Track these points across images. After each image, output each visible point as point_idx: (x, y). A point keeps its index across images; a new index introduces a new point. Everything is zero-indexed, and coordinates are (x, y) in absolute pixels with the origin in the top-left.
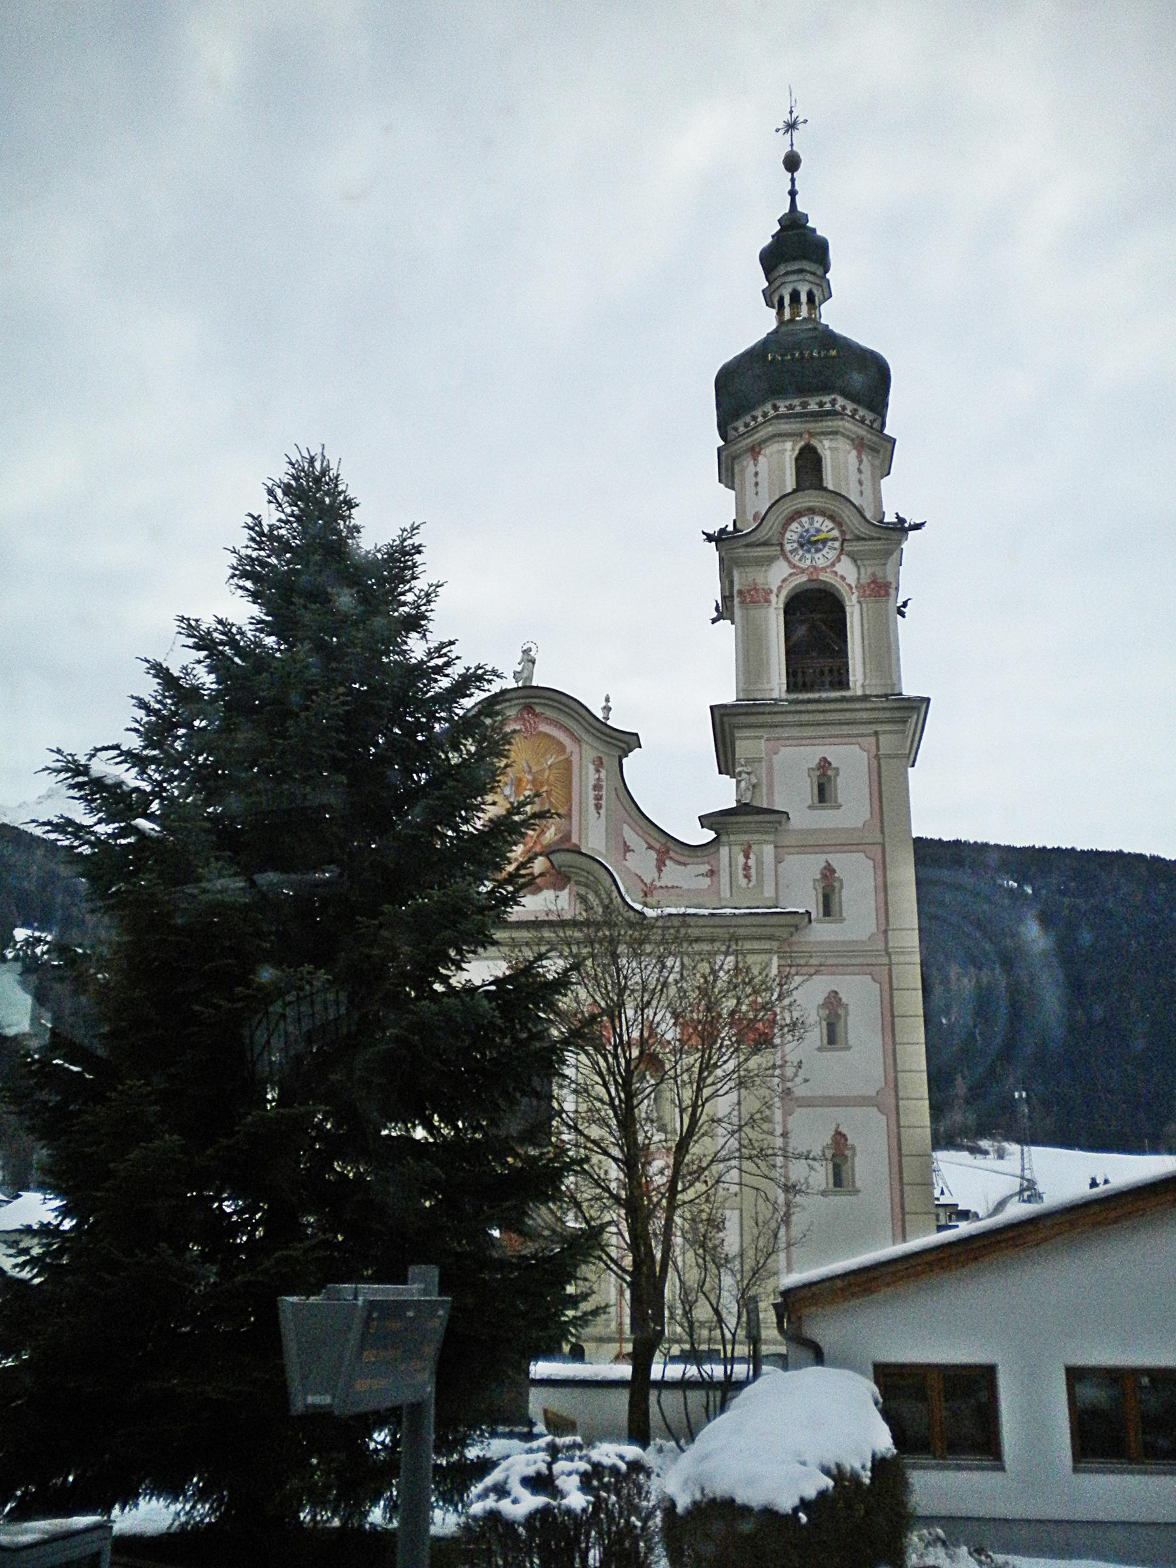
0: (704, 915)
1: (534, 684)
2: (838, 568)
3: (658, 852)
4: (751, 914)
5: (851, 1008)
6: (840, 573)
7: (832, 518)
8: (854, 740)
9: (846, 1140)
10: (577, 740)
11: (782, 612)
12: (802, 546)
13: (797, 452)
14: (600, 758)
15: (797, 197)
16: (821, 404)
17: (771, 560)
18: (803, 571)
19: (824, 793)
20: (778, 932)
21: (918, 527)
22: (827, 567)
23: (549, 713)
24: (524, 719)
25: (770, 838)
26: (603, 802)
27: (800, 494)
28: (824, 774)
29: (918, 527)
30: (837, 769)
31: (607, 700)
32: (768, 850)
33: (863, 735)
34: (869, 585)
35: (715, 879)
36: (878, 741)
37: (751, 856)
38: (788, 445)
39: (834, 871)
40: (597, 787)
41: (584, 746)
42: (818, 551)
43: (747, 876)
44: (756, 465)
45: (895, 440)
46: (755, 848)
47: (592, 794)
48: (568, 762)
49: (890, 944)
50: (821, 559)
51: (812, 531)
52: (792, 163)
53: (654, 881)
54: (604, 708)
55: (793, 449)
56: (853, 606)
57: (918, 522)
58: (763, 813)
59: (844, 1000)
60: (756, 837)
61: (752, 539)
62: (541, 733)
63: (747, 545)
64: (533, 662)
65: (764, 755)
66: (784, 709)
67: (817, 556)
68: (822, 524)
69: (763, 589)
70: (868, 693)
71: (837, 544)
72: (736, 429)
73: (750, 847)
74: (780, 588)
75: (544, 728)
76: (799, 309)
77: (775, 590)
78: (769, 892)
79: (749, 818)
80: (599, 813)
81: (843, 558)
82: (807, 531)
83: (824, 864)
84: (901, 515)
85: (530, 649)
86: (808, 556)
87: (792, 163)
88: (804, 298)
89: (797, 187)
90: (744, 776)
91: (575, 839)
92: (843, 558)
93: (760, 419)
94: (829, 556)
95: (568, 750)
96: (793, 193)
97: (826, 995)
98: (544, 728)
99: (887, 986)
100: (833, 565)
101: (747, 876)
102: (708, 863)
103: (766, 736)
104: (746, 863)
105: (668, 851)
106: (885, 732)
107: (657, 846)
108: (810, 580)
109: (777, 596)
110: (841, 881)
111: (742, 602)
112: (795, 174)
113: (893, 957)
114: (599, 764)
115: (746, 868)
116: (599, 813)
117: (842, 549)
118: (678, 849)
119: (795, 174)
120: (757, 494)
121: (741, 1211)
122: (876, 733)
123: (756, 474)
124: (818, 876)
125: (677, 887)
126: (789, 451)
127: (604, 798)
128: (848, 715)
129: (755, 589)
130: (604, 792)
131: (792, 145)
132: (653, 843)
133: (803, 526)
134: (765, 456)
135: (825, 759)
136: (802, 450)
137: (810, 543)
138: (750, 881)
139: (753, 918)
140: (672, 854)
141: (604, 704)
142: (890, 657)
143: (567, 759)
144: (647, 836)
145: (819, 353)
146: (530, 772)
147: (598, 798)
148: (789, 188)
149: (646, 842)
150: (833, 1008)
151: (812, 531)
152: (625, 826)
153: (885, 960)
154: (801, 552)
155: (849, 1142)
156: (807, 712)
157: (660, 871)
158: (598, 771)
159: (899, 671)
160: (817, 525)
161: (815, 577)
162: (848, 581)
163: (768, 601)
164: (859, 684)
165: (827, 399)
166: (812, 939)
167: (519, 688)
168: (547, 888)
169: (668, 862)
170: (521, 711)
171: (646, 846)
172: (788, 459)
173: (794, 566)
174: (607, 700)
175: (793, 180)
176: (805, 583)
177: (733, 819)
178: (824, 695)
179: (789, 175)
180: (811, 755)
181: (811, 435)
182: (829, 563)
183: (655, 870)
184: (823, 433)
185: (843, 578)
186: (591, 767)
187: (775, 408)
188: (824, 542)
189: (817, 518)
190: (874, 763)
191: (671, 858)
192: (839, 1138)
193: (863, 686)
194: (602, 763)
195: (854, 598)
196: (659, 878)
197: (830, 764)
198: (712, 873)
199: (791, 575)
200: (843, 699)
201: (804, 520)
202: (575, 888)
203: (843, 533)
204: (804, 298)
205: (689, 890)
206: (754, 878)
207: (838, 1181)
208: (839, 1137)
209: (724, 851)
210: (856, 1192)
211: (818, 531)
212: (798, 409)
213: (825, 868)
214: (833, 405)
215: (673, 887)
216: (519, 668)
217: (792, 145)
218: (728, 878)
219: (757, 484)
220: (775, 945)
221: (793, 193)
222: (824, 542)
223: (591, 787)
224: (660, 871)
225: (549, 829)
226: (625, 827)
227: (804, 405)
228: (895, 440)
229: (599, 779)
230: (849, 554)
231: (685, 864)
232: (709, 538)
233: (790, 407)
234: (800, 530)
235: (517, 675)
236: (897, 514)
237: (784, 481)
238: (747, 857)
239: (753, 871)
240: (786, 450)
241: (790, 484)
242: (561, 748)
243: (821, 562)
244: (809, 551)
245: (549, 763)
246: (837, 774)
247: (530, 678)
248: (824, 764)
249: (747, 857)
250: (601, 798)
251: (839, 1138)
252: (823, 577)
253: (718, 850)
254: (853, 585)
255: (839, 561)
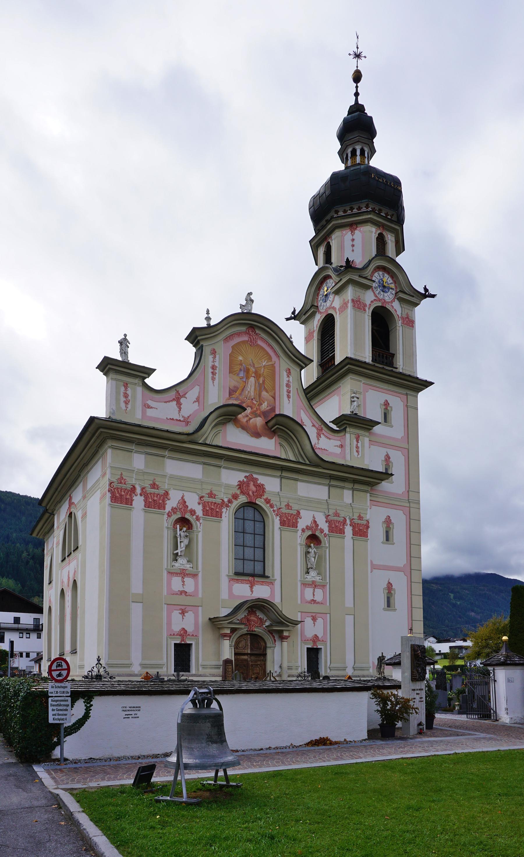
2: (394, 304)
3: (317, 429)
5: (395, 524)
6: (370, 303)
13: (377, 235)
24: (250, 335)
26: (291, 394)
29: (433, 296)
31: (208, 312)
32: (367, 440)
35: (343, 448)
43: (357, 451)
48: (273, 366)
52: (357, 77)
54: (206, 318)
69: (363, 303)
75: (260, 342)
76: (355, 159)
80: (289, 400)
84: (427, 287)
87: (357, 77)
88: (358, 153)
95: (273, 360)
96: (357, 94)
98: (260, 342)
107: (317, 426)
112: (358, 84)
113: (411, 504)
115: (357, 447)
116: (289, 400)
118: (326, 430)
120: (353, 251)
123: (353, 240)
124: (384, 459)
125: (326, 450)
127: (291, 392)
129: (359, 301)
131: (357, 67)
134: (360, 231)
137: (384, 288)
138: (358, 454)
140: (323, 432)
141: (206, 316)
143: (273, 365)
147: (289, 392)
148: (355, 91)
152: (302, 410)
153: (408, 505)
157: (318, 439)
158: (288, 376)
168: (264, 436)
169: (322, 435)
171: (312, 425)
173: (376, 296)
174: (208, 312)
175: (357, 87)
179: (355, 85)
183: (316, 439)
186: (285, 374)
190: (406, 408)
191: (323, 434)
194: (290, 372)
198: (342, 446)
199: (375, 300)
204: (358, 153)
206: (360, 453)
213: (386, 455)
215: (324, 449)
217: (357, 67)
218: (349, 451)
221: (357, 94)
224: (318, 439)
226: (302, 411)
229: (289, 381)
231: (330, 439)
235: (242, 307)
236: (425, 286)
238: (358, 442)
239: (360, 450)
242: (270, 358)
249: (358, 442)
253: (345, 435)
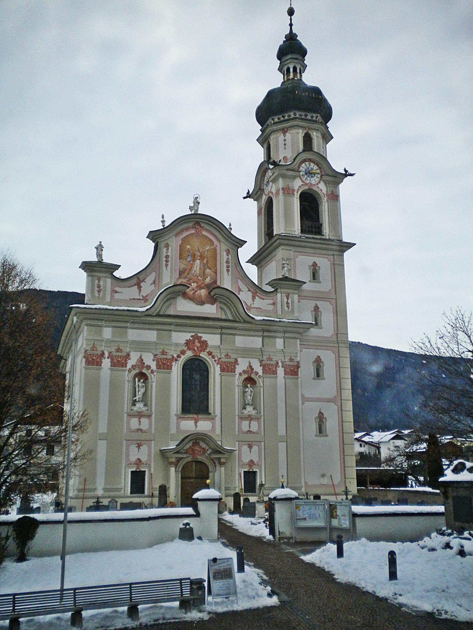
0: (277, 321)
1: (199, 213)
2: (319, 185)
3: (253, 293)
4: (269, 320)
5: (325, 363)
7: (318, 165)
8: (326, 256)
9: (323, 415)
10: (219, 240)
11: (299, 200)
12: (306, 174)
14: (228, 250)
15: (293, 27)
16: (312, 117)
17: (295, 177)
18: (306, 184)
19: (315, 276)
20: (301, 330)
21: (352, 175)
22: (315, 184)
23: (207, 227)
25: (296, 292)
27: (304, 153)
28: (314, 269)
29: (352, 175)
30: (319, 267)
31: (163, 217)
32: (296, 297)
33: (329, 255)
34: (331, 194)
35: (275, 306)
36: (334, 258)
37: (290, 298)
38: (301, 131)
39: (318, 308)
40: (227, 262)
41: (221, 243)
42: (312, 177)
44: (285, 137)
45: (333, 138)
46: (290, 295)
47: (225, 265)
48: (215, 249)
49: (339, 339)
50: (314, 180)
51: (310, 169)
53: (251, 305)
55: (302, 133)
56: (325, 202)
57: (352, 173)
58: (289, 281)
59: (323, 360)
60: (292, 291)
61: (289, 167)
62: (203, 235)
63: (288, 170)
64: (199, 203)
65: (292, 257)
66: (303, 240)
67: (312, 179)
68: (315, 167)
70: (330, 238)
71: (319, 176)
72: (273, 119)
73: (289, 295)
74: (298, 190)
75: (204, 233)
77: (296, 190)
78: (296, 314)
79: (288, 283)
81: (321, 182)
82: (308, 168)
83: (315, 305)
84: (347, 169)
85: (197, 198)
86: (309, 178)
89: (293, 22)
90: (286, 265)
91: (218, 283)
92: (321, 182)
93: (286, 117)
94: (316, 180)
95: (215, 244)
96: (291, 25)
97: (316, 357)
98: (204, 233)
99: (337, 356)
100: (318, 184)
101: (288, 307)
102: (272, 299)
103: (293, 250)
104: (287, 301)
105: (256, 293)
106: (336, 255)
107: (252, 290)
108: (309, 189)
109: (297, 193)
110: (321, 312)
111: (284, 193)
114: (228, 252)
115: (288, 303)
117: (321, 178)
119: (292, 17)
121: (287, 442)
122: (333, 255)
123: (285, 140)
124: (313, 310)
126: (300, 134)
128: (327, 246)
130: (230, 264)
131: (291, 4)
132: (251, 289)
133: (306, 166)
135: (315, 262)
136: (305, 134)
137: (309, 173)
139: (295, 324)
140: (258, 294)
141: (162, 219)
142: (338, 224)
144: (248, 285)
145: (315, 95)
146: (199, 251)
147: (228, 267)
148: (289, 23)
149: (155, 278)
150: (318, 363)
151: (310, 169)
154: (306, 176)
155: (324, 416)
156: (325, 244)
157: (253, 301)
158: (228, 255)
159: (341, 231)
160: (312, 166)
161: (311, 187)
162: (323, 192)
163: (293, 194)
164: (327, 234)
165: (314, 115)
166: (308, 334)
167: (192, 214)
168: (208, 303)
169: (256, 297)
170: (194, 224)
172: (300, 137)
175: (291, 19)
176: (306, 190)
177: (280, 282)
178: (314, 236)
180: (310, 260)
181: (309, 128)
182: (316, 183)
184: (315, 129)
185: (321, 190)
187: (295, 114)
188: (315, 174)
189: (312, 164)
190: (333, 267)
192: (321, 414)
193: (329, 235)
195: (325, 198)
196: (253, 304)
197: (317, 265)
198: (274, 304)
199: (302, 185)
200: (322, 239)
201: (307, 163)
202: (220, 305)
203: (321, 171)
204: (291, 70)
205: (265, 310)
206: (290, 308)
207: (320, 431)
208: (320, 414)
209: (279, 295)
210: (327, 436)
211: (312, 169)
212: (303, 117)
213: (315, 306)
214: (316, 118)
216: (192, 205)
217: (291, 4)
219: (285, 145)
220: (298, 336)
221: (291, 25)
222: (315, 174)
223: (225, 262)
224: (253, 301)
225: (207, 277)
227: (306, 116)
228: (333, 138)
229: (228, 259)
230: (323, 181)
231: (263, 299)
232: (346, 174)
233: (301, 115)
234: (305, 167)
237: (299, 146)
238: (288, 299)
239: (290, 305)
240: (299, 133)
241: (301, 148)
242: (212, 243)
243: (313, 182)
244: (309, 177)
245: (207, 249)
246: (319, 269)
247: (197, 210)
248: (315, 264)
249: (288, 299)
250: (229, 267)
251: (321, 414)
252: (314, 188)
253: (276, 295)
254: (325, 194)
255: (320, 183)
